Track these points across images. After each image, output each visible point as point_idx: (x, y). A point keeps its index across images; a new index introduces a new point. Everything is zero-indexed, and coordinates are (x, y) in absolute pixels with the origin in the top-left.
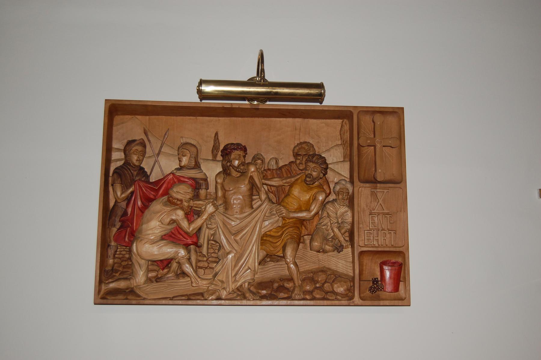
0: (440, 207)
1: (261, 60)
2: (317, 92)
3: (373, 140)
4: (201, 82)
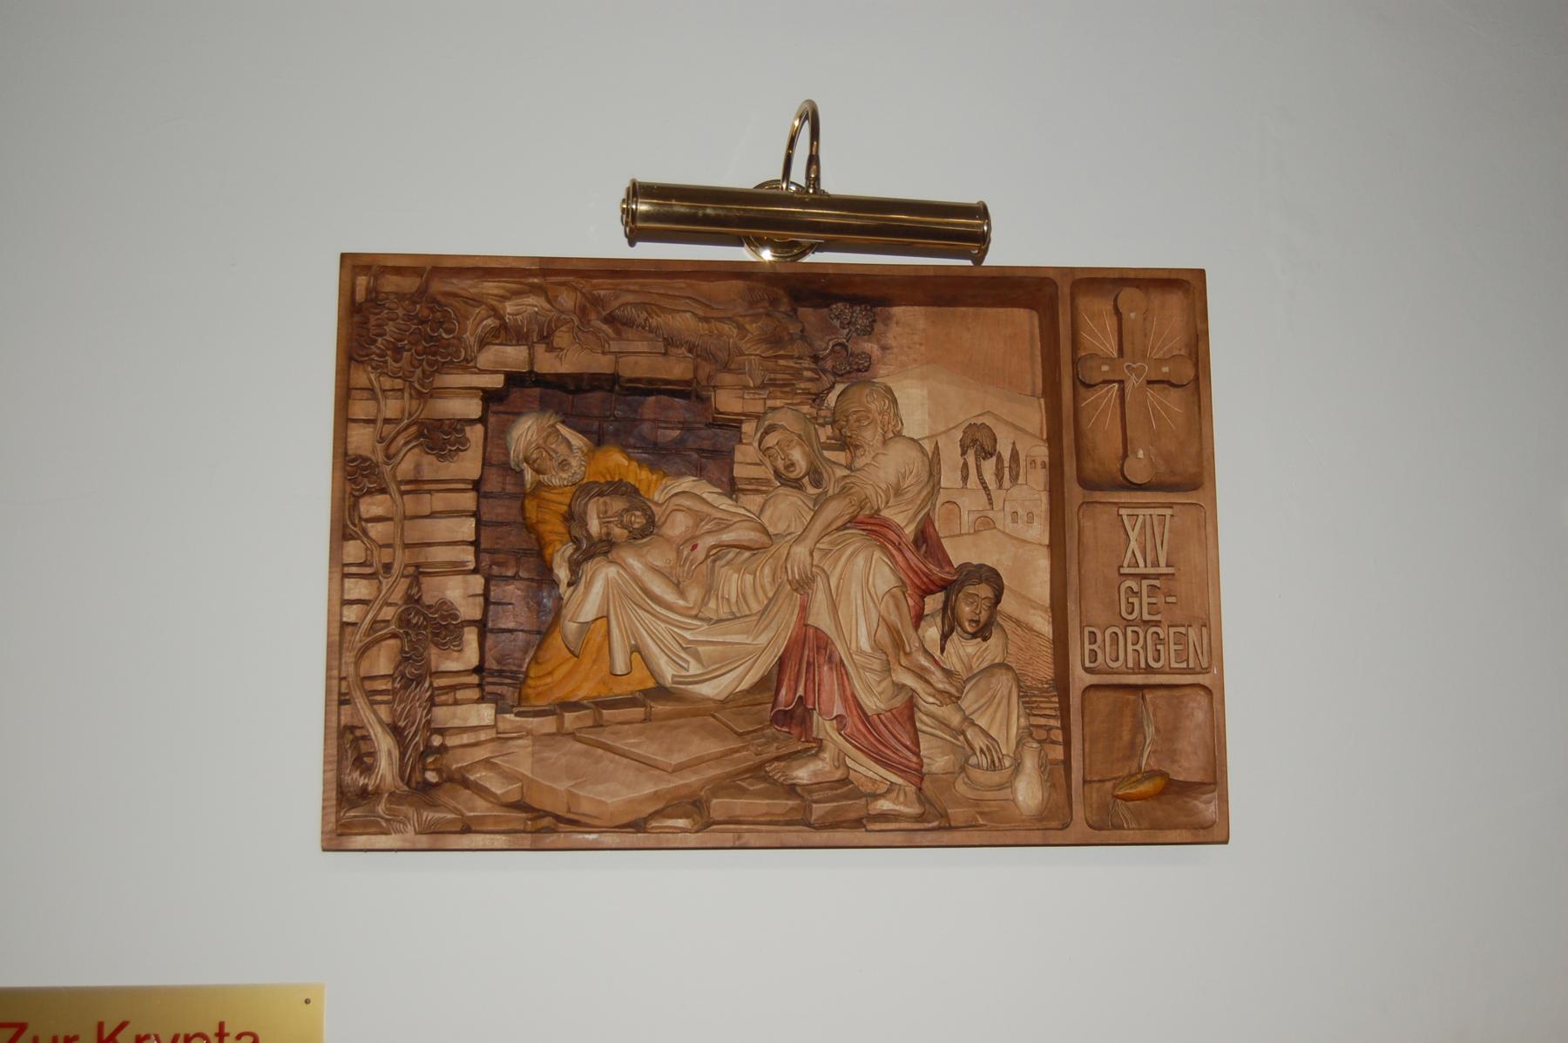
0: (1307, 559)
1: (811, 116)
2: (961, 226)
3: (1112, 370)
4: (638, 191)
